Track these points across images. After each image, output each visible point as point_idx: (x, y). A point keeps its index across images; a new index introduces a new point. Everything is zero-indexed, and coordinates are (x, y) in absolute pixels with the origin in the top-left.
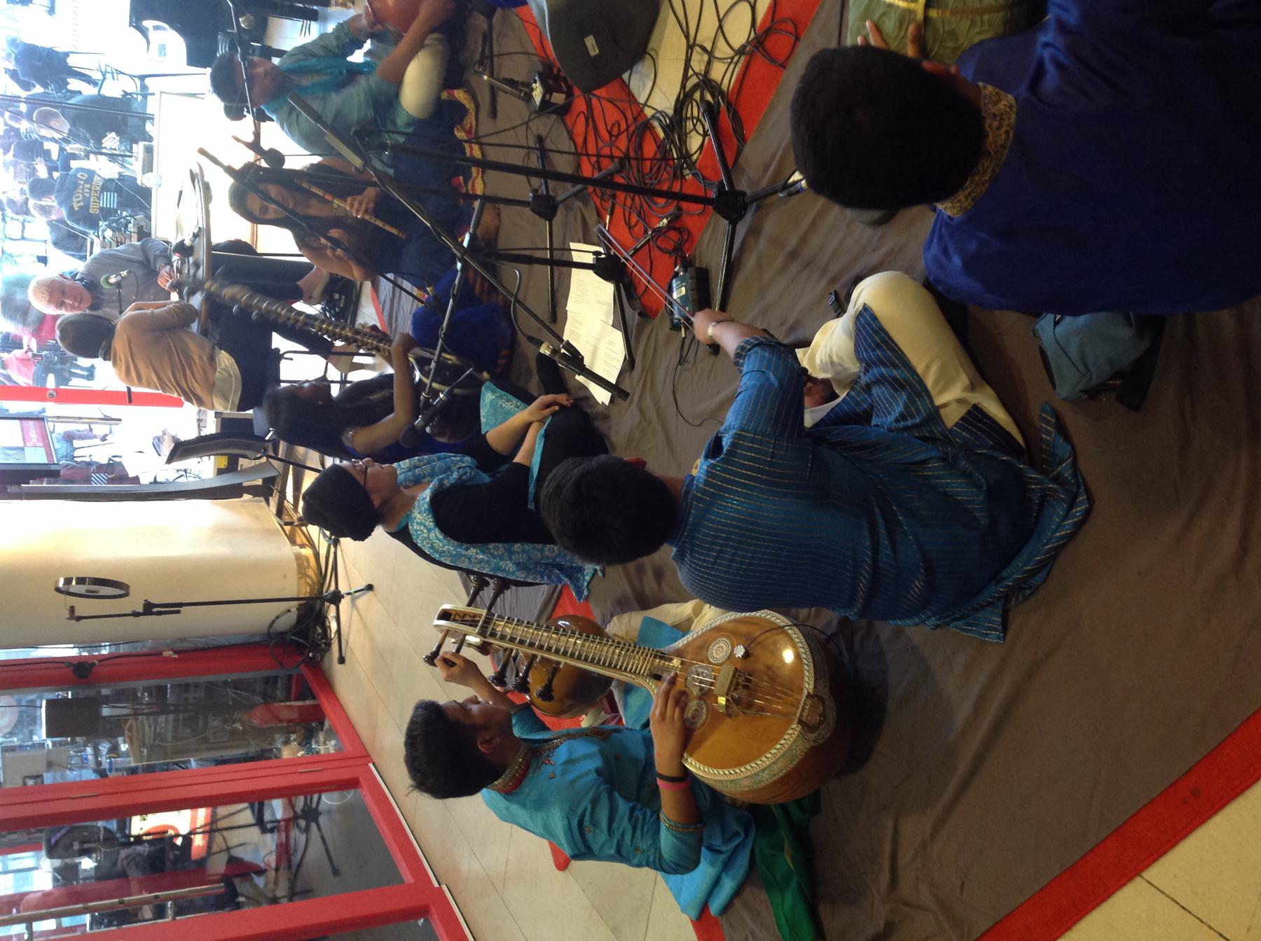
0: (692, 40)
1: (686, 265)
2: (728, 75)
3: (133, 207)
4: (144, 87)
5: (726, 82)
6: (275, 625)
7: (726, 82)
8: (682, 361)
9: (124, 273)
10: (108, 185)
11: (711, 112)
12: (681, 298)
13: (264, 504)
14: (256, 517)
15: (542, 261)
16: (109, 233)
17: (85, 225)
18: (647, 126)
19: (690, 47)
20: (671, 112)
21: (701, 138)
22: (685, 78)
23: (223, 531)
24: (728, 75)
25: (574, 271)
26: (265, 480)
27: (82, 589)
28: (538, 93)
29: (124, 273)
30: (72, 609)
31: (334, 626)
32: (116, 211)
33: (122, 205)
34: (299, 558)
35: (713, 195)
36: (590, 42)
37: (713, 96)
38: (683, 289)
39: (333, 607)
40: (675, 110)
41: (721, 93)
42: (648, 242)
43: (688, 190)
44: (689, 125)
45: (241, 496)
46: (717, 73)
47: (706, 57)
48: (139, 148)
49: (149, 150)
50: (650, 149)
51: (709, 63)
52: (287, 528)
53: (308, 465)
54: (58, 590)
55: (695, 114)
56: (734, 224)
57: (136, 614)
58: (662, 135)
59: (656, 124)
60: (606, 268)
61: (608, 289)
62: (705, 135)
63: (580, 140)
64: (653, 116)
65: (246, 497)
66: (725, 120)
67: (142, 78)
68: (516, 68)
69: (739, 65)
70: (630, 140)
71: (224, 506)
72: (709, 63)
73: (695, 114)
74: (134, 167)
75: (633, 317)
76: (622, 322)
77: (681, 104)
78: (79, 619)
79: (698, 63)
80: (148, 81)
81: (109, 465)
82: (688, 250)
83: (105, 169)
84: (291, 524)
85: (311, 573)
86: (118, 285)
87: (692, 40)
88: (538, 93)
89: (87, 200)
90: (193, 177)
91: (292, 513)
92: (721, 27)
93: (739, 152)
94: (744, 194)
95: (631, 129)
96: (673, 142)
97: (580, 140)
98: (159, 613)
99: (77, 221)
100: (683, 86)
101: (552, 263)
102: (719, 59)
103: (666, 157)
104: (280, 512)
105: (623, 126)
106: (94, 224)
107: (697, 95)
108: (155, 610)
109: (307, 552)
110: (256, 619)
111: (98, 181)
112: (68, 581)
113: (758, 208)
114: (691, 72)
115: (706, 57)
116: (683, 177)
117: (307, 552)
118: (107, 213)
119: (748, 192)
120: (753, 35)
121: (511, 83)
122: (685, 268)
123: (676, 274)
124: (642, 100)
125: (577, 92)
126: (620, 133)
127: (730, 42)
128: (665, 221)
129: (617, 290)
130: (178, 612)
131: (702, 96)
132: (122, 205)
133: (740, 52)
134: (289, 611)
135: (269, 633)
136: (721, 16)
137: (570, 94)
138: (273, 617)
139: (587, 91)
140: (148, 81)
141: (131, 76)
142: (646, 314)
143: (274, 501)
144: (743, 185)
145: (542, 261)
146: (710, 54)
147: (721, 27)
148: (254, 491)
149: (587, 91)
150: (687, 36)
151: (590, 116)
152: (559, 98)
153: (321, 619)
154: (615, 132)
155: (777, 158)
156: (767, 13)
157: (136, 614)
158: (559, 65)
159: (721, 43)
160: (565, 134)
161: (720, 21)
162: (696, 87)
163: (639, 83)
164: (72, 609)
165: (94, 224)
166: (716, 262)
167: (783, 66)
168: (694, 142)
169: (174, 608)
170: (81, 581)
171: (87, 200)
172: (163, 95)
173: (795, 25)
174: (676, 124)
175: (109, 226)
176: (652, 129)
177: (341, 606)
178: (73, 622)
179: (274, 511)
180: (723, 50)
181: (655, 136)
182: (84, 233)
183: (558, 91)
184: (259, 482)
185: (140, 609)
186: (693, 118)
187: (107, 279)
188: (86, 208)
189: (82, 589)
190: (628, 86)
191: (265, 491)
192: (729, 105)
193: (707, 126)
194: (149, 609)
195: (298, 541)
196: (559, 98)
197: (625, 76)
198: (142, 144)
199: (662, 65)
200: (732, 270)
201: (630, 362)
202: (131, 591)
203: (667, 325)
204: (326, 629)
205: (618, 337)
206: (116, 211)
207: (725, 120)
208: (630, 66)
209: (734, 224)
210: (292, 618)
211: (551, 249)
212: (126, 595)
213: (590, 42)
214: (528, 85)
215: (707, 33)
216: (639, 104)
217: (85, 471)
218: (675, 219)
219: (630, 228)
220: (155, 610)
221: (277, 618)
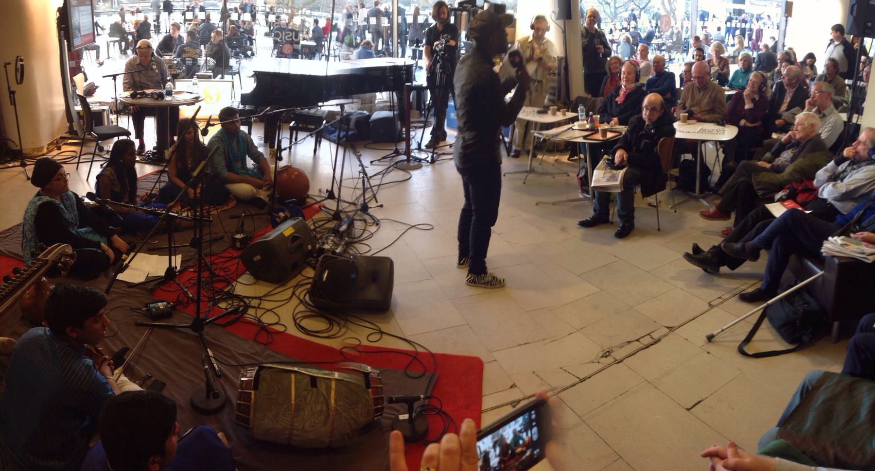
0: (263, 298)
1: (173, 307)
2: (250, 316)
3: (187, 71)
4: (235, 74)
5: (247, 316)
6: (10, 142)
7: (247, 316)
8: (132, 309)
9: (157, 71)
10: (195, 61)
11: (235, 311)
12: (159, 307)
13: (66, 131)
14: (59, 129)
15: (170, 244)
16: (176, 62)
17: (179, 52)
18: (229, 283)
19: (260, 298)
20: (235, 293)
21: (225, 307)
22: (248, 298)
23: (52, 115)
24: (250, 316)
25: (168, 257)
26: (76, 131)
27: (19, 66)
28: (238, 236)
29: (157, 71)
30: (9, 64)
31: (11, 165)
32: (185, 64)
33: (188, 67)
34: (42, 148)
35: (201, 316)
36: (258, 257)
37: (242, 310)
38: (162, 307)
39: (19, 164)
40: (236, 295)
41: (243, 314)
42: (182, 289)
43: (202, 305)
44: (230, 302)
45: (68, 122)
46: (251, 311)
47: (257, 306)
48: (210, 73)
49: (209, 77)
50: (219, 286)
51: (254, 307)
52: (55, 142)
53: (83, 148)
54: (18, 57)
55: (235, 304)
56: (190, 327)
57: (9, 88)
58: (226, 290)
59: (230, 287)
60: (170, 270)
61: (162, 273)
62: (226, 309)
63: (222, 255)
64: (233, 286)
65: (68, 124)
66: (233, 317)
67: (239, 73)
68: (248, 225)
69: (254, 321)
70: (223, 276)
71: (64, 115)
72: (254, 307)
73: (235, 304)
74: (202, 72)
75: (150, 286)
76: (149, 280)
77: (239, 298)
78: (5, 67)
79: (254, 303)
80: (237, 75)
81: (80, 66)
82: (180, 307)
83: (201, 61)
84: (57, 143)
85: (35, 153)
86: (152, 69)
87: (263, 298)
88: (238, 236)
89: (188, 52)
90: (197, 98)
91: (63, 143)
92: (268, 310)
93: (219, 325)
94: (203, 330)
95: (228, 277)
96: (223, 295)
97: (222, 255)
98: (10, 97)
99: (180, 48)
100: (245, 297)
101: (170, 247)
102: (256, 311)
103: (218, 293)
104: (62, 138)
105: (228, 273)
106: (179, 56)
107: (242, 304)
108: (12, 95)
109: (45, 151)
110: (12, 134)
111: (196, 57)
112: (22, 60)
113: (197, 337)
114: (250, 300)
115: (257, 306)
116: (209, 301)
117: (45, 151)
118: (184, 61)
119: (203, 332)
120: (265, 325)
121: (242, 226)
122: (172, 307)
123: (169, 303)
124: (238, 280)
125: (240, 253)
126: (225, 272)
127: (409, 231)
128: (191, 296)
129: (159, 278)
130: (11, 104)
131: (242, 306)
132: (188, 67)
133: (260, 321)
134: (17, 146)
135: (7, 139)
136: (273, 310)
137: (239, 249)
138: (14, 140)
139: (241, 257)
140: (237, 75)
141: (239, 68)
142: (152, 291)
143: (67, 135)
144: (206, 329)
145: (170, 244)
146: (258, 307)
147: (268, 310)
148: (71, 127)
149: (241, 257)
150: (264, 296)
151: (232, 258)
152: (238, 245)
153: (14, 159)
154: (225, 270)
155: (218, 343)
156: (274, 330)
157: (9, 88)
158: (251, 244)
159: (263, 311)
160: (225, 248)
161: (414, 226)
162: (245, 302)
163: (246, 278)
164: (9, 64)
165: (179, 56)
166: (175, 322)
167: (255, 340)
168: (223, 305)
169: (13, 102)
170: (22, 66)
171: (188, 52)
172: (231, 83)
173: (271, 343)
174: (231, 296)
175: (178, 62)
176: (228, 286)
177: (20, 168)
178: (3, 65)
179: (63, 136)
180: (260, 312)
181: (225, 287)
182: (175, 52)
183: (240, 245)
184: (75, 129)
185: (11, 90)
186: (233, 303)
187: (154, 65)
188: (185, 52)
189: (19, 66)
190: (244, 274)
191: (72, 132)
192: (239, 318)
193: (230, 310)
194: (12, 93)
195: (50, 147)
196: (238, 245)
197: (248, 272)
198: (212, 74)
199: (253, 287)
200: (172, 328)
201: (131, 285)
202: (20, 85)
203: (147, 302)
204: (9, 162)
205: (142, 279)
206: (185, 64)
207: (233, 317)
208: (251, 274)
209: (190, 327)
210: (14, 148)
211: (175, 247)
212: (18, 84)
213: (258, 257)
214: (242, 232)
215: (267, 305)
216: (237, 278)
217: (76, 56)
218: (192, 299)
219: (188, 280)
220: (12, 95)
221: (14, 142)
